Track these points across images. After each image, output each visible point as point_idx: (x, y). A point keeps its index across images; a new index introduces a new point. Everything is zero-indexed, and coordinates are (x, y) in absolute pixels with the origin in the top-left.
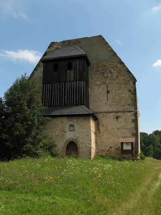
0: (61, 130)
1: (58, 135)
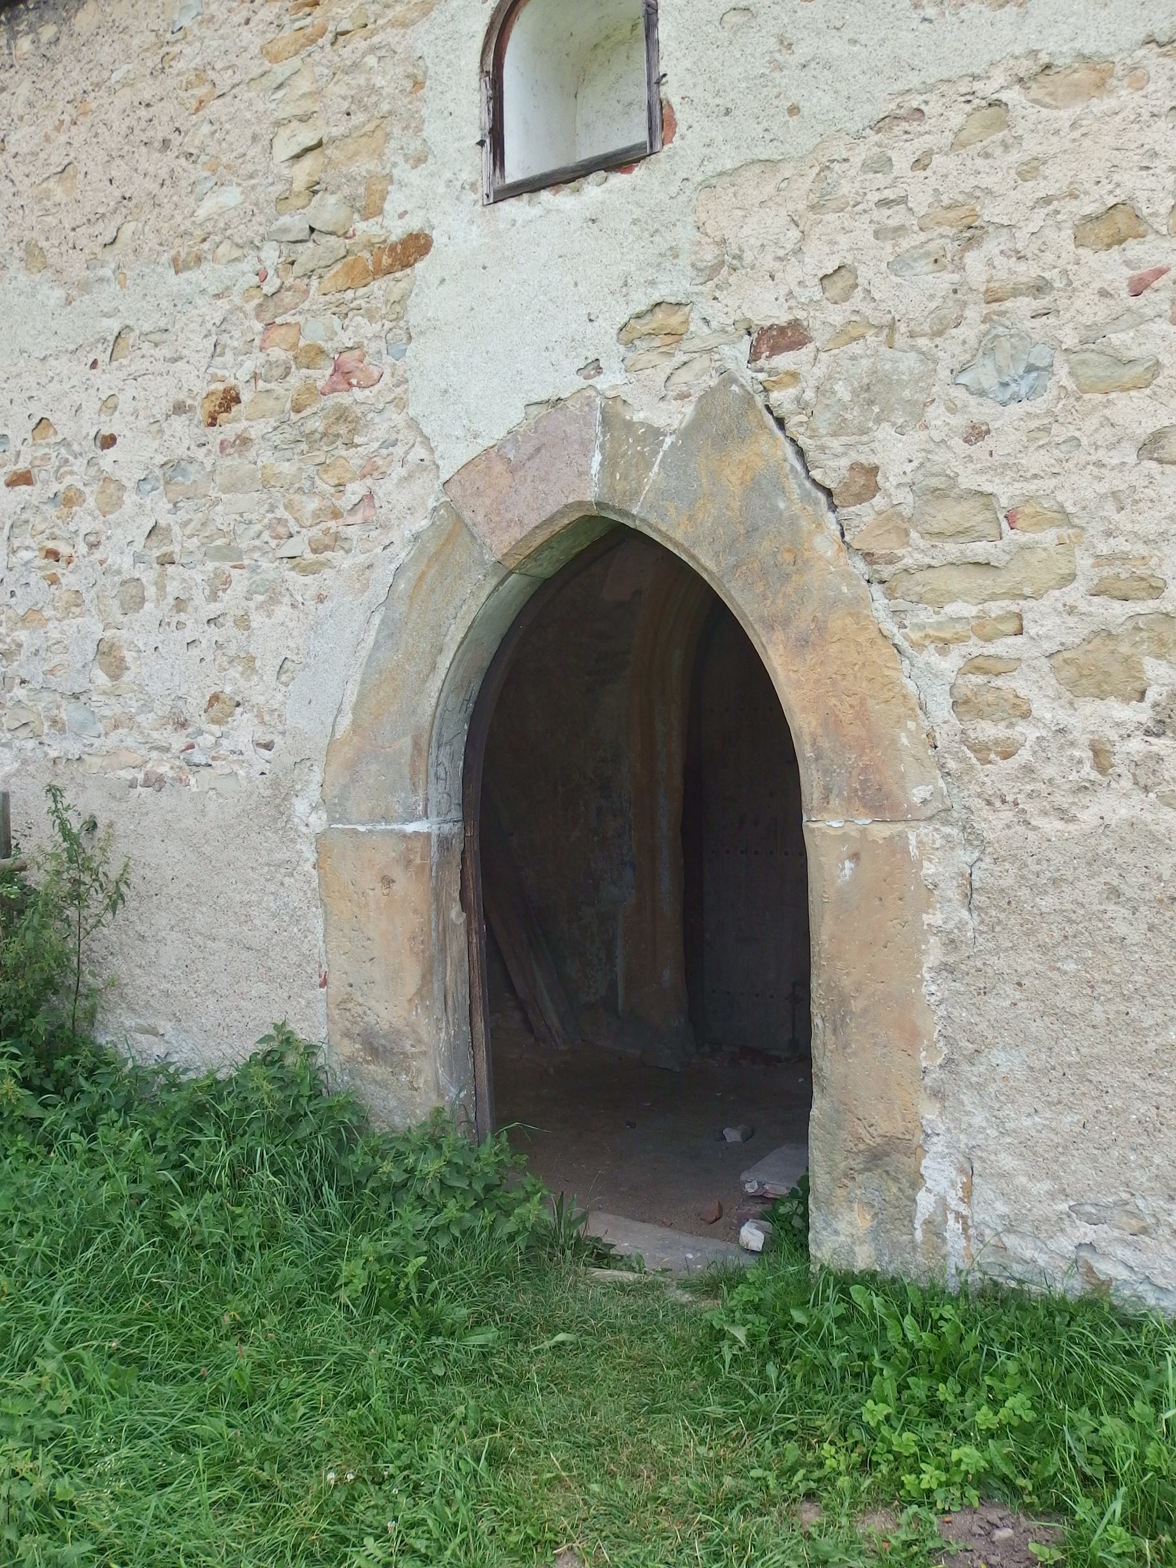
0: (295, 223)
1: (230, 399)
